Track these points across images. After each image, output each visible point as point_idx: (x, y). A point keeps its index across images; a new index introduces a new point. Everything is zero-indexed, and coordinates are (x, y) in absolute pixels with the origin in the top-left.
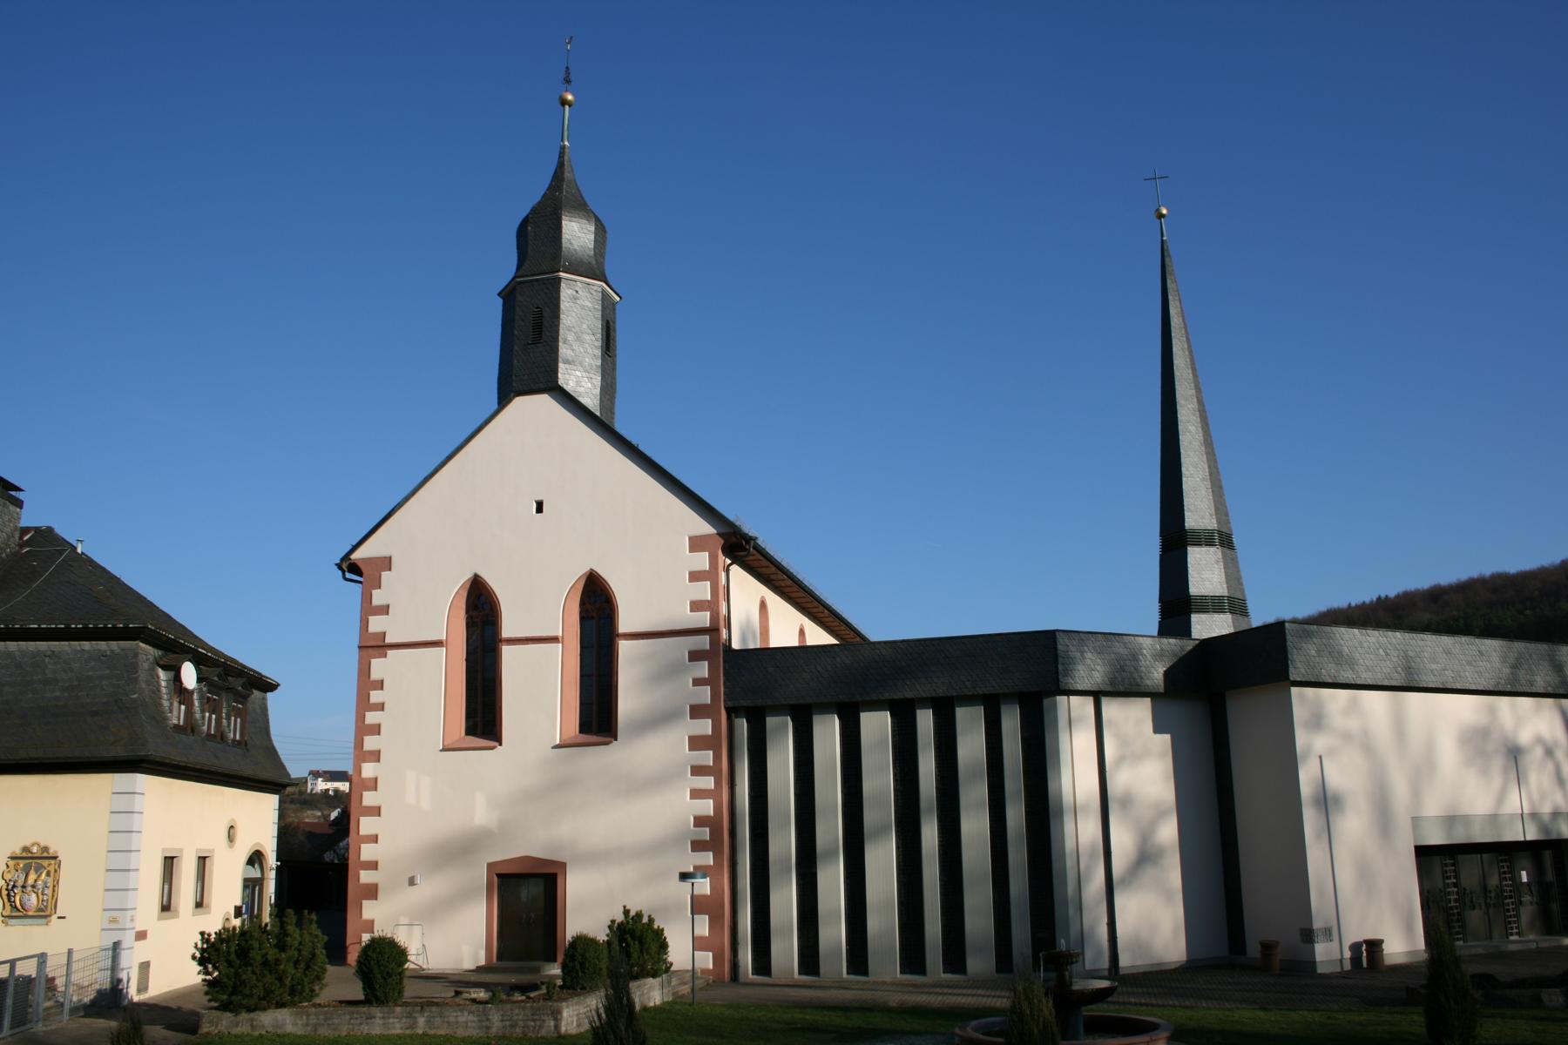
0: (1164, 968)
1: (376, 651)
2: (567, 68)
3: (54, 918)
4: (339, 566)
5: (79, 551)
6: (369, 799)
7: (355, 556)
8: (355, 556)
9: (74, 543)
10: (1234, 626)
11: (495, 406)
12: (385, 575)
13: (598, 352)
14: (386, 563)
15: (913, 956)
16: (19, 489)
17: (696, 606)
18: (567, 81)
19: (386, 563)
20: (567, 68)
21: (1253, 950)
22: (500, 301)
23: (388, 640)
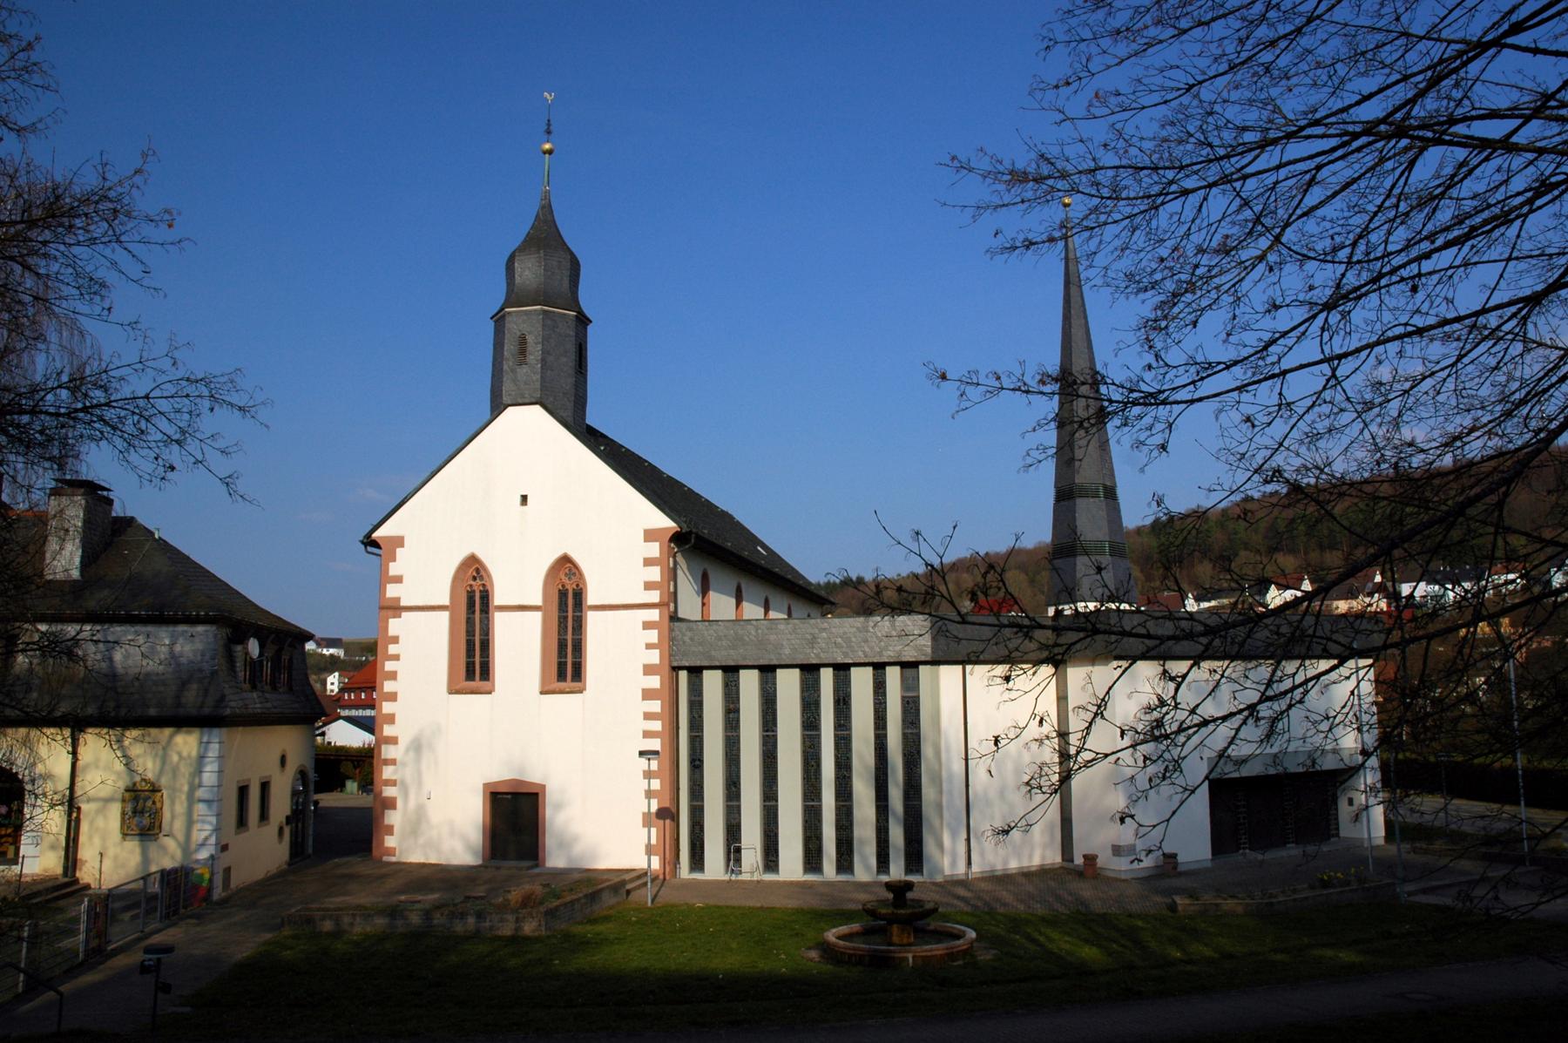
0: (955, 878)
1: (390, 613)
2: (549, 124)
3: (161, 835)
4: (362, 542)
5: (157, 536)
6: (392, 649)
7: (376, 535)
8: (376, 535)
9: (153, 530)
10: (938, 671)
11: (488, 416)
12: (399, 550)
13: (572, 372)
14: (399, 541)
15: (812, 859)
16: (109, 490)
17: (649, 586)
18: (549, 132)
19: (399, 541)
20: (549, 124)
21: (1079, 860)
22: (492, 323)
23: (403, 603)
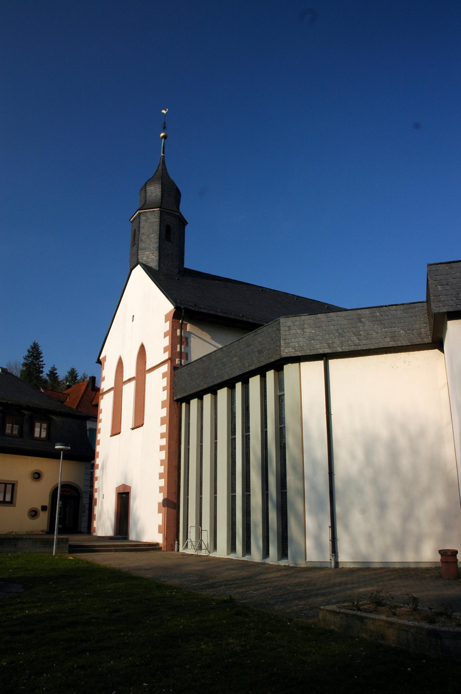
2: (165, 123)
18: (164, 128)
20: (165, 123)
